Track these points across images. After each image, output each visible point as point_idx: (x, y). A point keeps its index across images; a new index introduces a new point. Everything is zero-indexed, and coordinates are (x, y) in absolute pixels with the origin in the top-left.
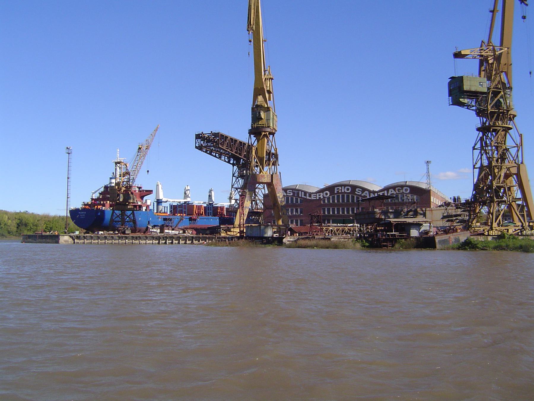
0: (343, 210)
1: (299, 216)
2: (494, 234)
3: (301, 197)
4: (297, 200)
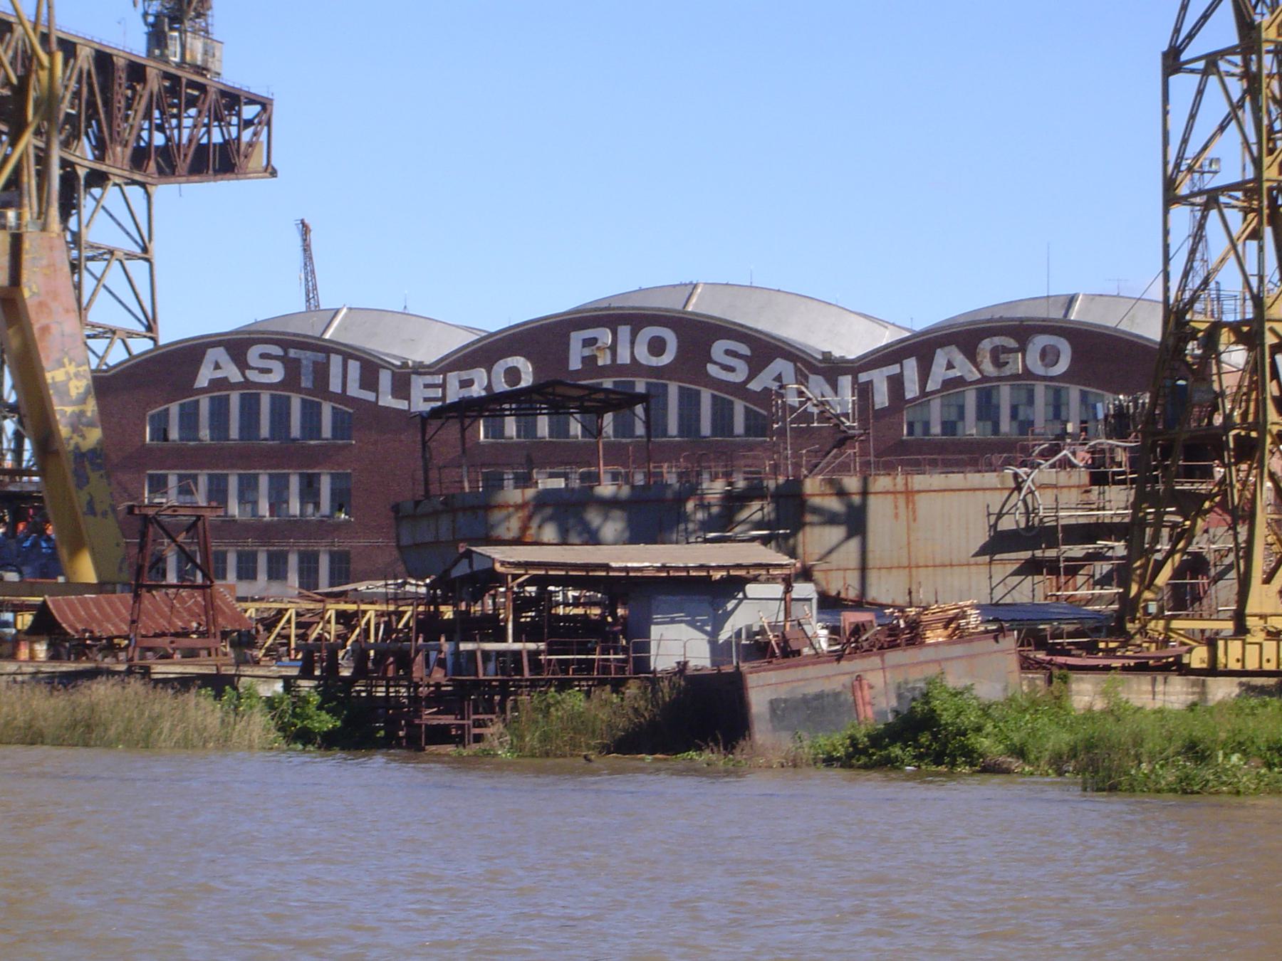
0: (248, 486)
1: (325, 528)
2: (1252, 665)
3: (343, 398)
4: (311, 414)
